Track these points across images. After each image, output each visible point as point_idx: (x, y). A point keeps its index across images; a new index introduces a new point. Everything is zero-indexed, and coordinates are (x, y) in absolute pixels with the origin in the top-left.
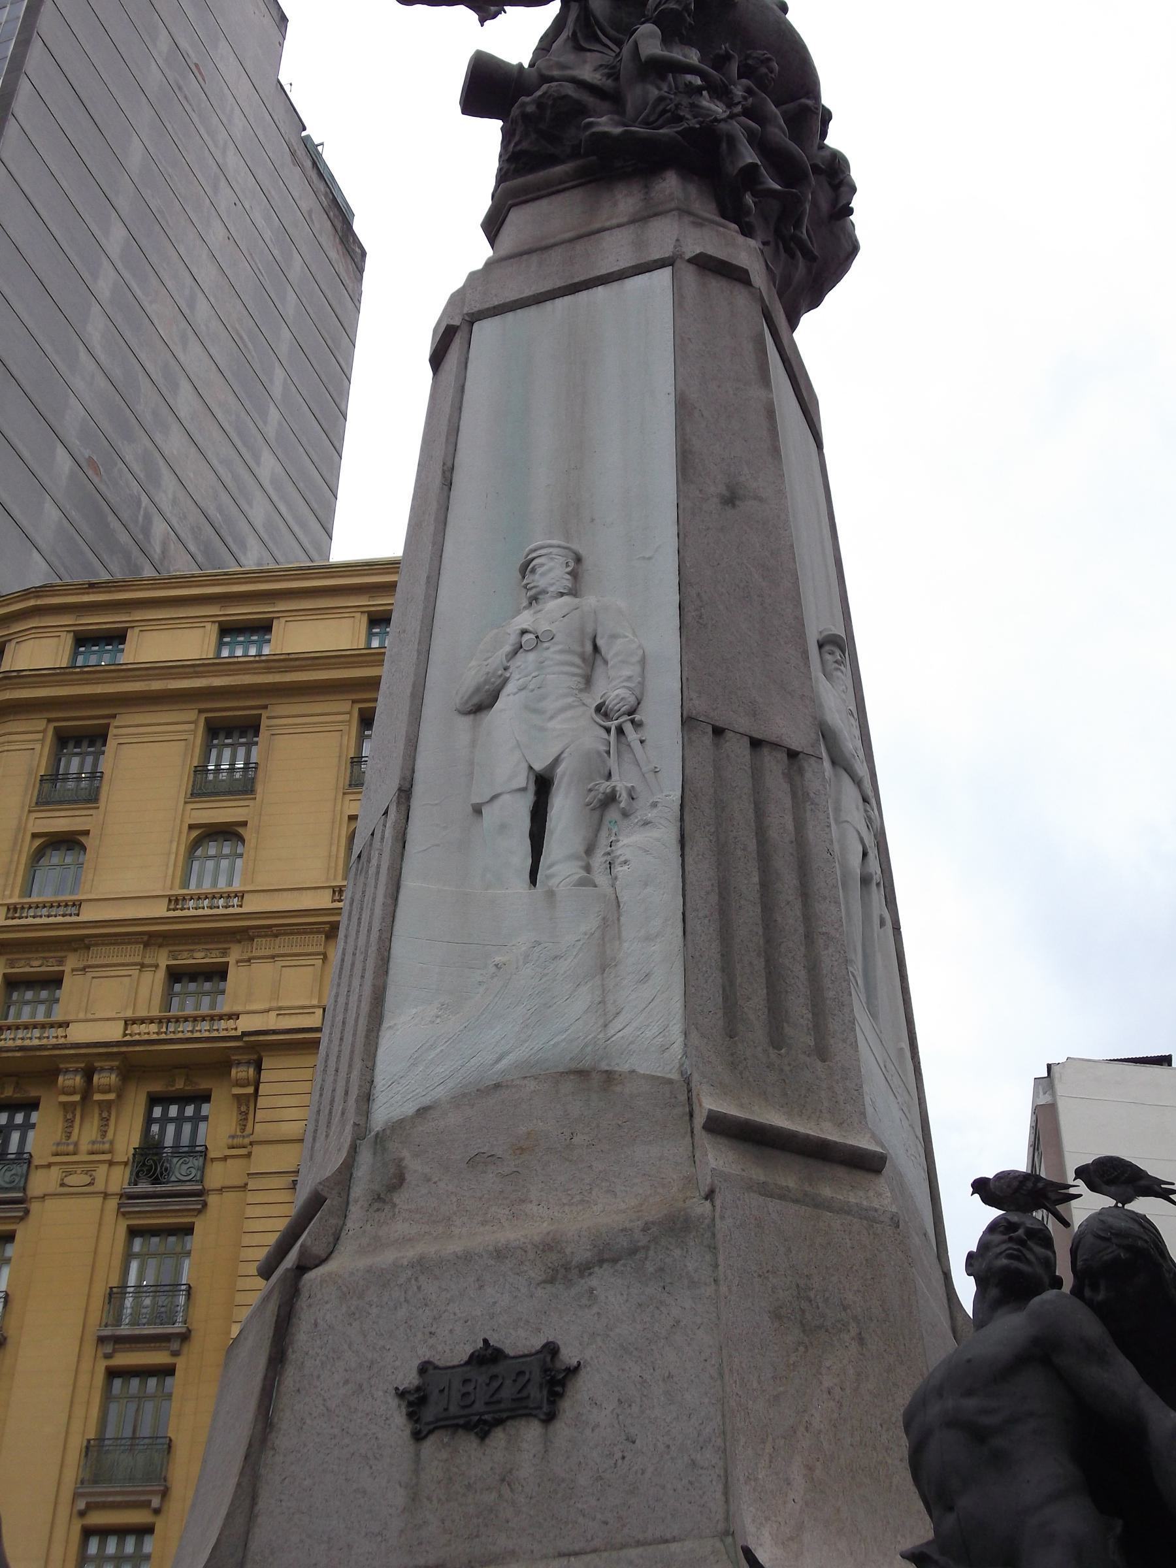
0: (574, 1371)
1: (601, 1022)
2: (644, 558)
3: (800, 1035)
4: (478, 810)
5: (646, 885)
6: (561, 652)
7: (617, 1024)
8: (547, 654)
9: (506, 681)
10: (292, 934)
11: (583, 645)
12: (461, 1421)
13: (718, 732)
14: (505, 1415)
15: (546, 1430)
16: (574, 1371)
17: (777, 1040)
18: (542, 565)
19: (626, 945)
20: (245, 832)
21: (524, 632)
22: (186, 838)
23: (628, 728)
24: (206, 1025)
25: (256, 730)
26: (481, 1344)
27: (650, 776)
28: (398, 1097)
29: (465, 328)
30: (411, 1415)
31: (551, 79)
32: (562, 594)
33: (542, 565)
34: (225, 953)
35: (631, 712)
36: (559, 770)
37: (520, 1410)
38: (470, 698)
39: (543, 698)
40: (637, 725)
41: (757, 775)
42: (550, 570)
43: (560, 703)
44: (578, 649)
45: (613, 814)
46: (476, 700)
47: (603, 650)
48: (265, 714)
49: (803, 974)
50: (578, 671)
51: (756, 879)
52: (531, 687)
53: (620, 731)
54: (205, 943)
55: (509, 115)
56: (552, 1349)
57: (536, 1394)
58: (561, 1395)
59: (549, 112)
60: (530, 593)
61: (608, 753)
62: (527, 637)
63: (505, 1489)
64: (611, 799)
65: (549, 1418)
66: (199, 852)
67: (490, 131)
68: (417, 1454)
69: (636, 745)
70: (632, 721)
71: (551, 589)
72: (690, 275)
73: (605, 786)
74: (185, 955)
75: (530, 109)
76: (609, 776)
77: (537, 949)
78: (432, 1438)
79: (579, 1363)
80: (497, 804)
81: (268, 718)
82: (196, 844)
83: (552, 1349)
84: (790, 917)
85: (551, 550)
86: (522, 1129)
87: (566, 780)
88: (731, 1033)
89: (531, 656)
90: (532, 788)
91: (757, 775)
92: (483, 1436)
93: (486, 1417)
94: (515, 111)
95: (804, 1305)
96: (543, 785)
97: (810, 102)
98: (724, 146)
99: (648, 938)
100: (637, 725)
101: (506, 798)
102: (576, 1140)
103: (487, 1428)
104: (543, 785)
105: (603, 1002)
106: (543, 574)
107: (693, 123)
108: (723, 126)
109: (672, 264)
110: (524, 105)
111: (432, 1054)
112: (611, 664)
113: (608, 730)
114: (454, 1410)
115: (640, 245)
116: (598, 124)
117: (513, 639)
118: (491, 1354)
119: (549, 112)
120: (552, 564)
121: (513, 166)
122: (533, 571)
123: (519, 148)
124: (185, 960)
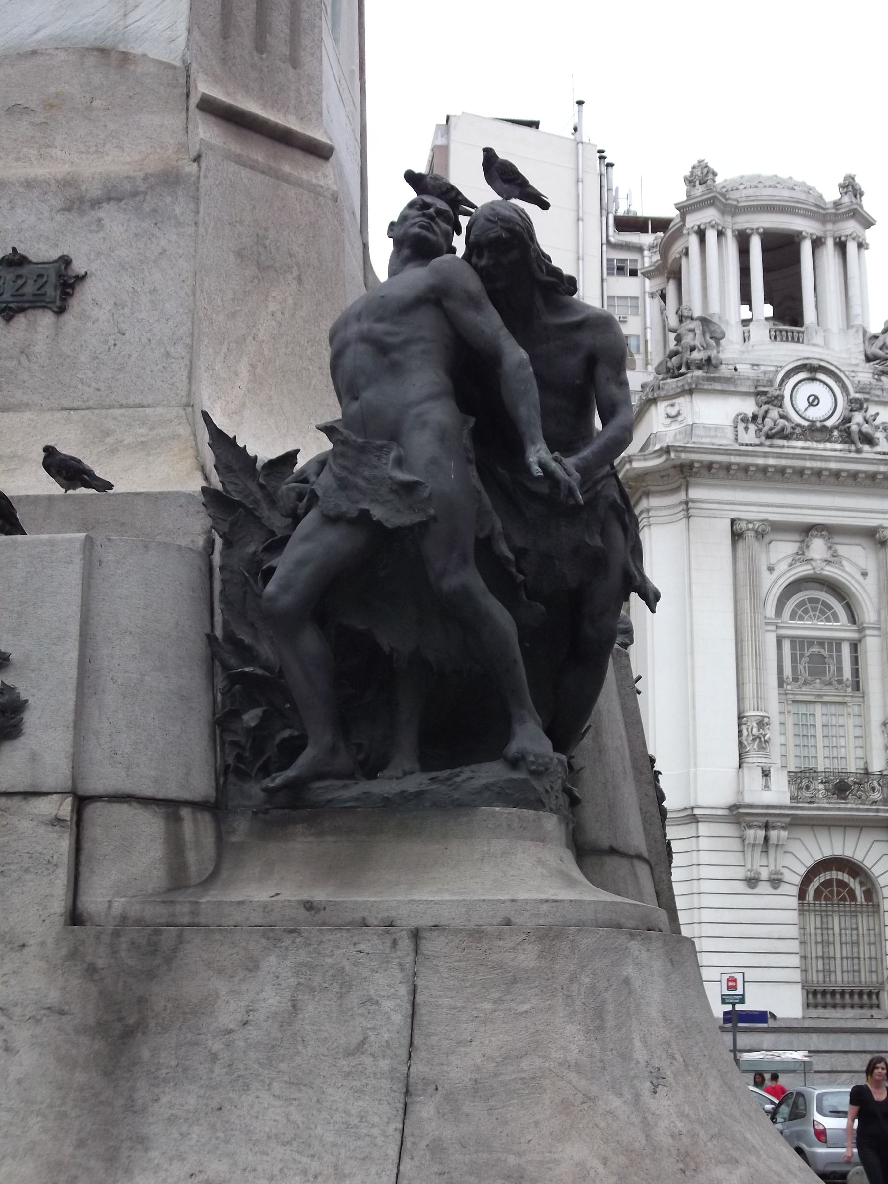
0: (81, 278)
1: (122, 12)
7: (134, 16)
14: (26, 305)
16: (81, 278)
26: (10, 251)
37: (38, 303)
56: (65, 261)
58: (70, 295)
63: (23, 359)
65: (61, 311)
79: (86, 273)
83: (65, 261)
86: (52, 90)
88: (225, 35)
93: (11, 305)
95: (261, 249)
102: (97, 103)
103: (11, 314)
118: (18, 259)
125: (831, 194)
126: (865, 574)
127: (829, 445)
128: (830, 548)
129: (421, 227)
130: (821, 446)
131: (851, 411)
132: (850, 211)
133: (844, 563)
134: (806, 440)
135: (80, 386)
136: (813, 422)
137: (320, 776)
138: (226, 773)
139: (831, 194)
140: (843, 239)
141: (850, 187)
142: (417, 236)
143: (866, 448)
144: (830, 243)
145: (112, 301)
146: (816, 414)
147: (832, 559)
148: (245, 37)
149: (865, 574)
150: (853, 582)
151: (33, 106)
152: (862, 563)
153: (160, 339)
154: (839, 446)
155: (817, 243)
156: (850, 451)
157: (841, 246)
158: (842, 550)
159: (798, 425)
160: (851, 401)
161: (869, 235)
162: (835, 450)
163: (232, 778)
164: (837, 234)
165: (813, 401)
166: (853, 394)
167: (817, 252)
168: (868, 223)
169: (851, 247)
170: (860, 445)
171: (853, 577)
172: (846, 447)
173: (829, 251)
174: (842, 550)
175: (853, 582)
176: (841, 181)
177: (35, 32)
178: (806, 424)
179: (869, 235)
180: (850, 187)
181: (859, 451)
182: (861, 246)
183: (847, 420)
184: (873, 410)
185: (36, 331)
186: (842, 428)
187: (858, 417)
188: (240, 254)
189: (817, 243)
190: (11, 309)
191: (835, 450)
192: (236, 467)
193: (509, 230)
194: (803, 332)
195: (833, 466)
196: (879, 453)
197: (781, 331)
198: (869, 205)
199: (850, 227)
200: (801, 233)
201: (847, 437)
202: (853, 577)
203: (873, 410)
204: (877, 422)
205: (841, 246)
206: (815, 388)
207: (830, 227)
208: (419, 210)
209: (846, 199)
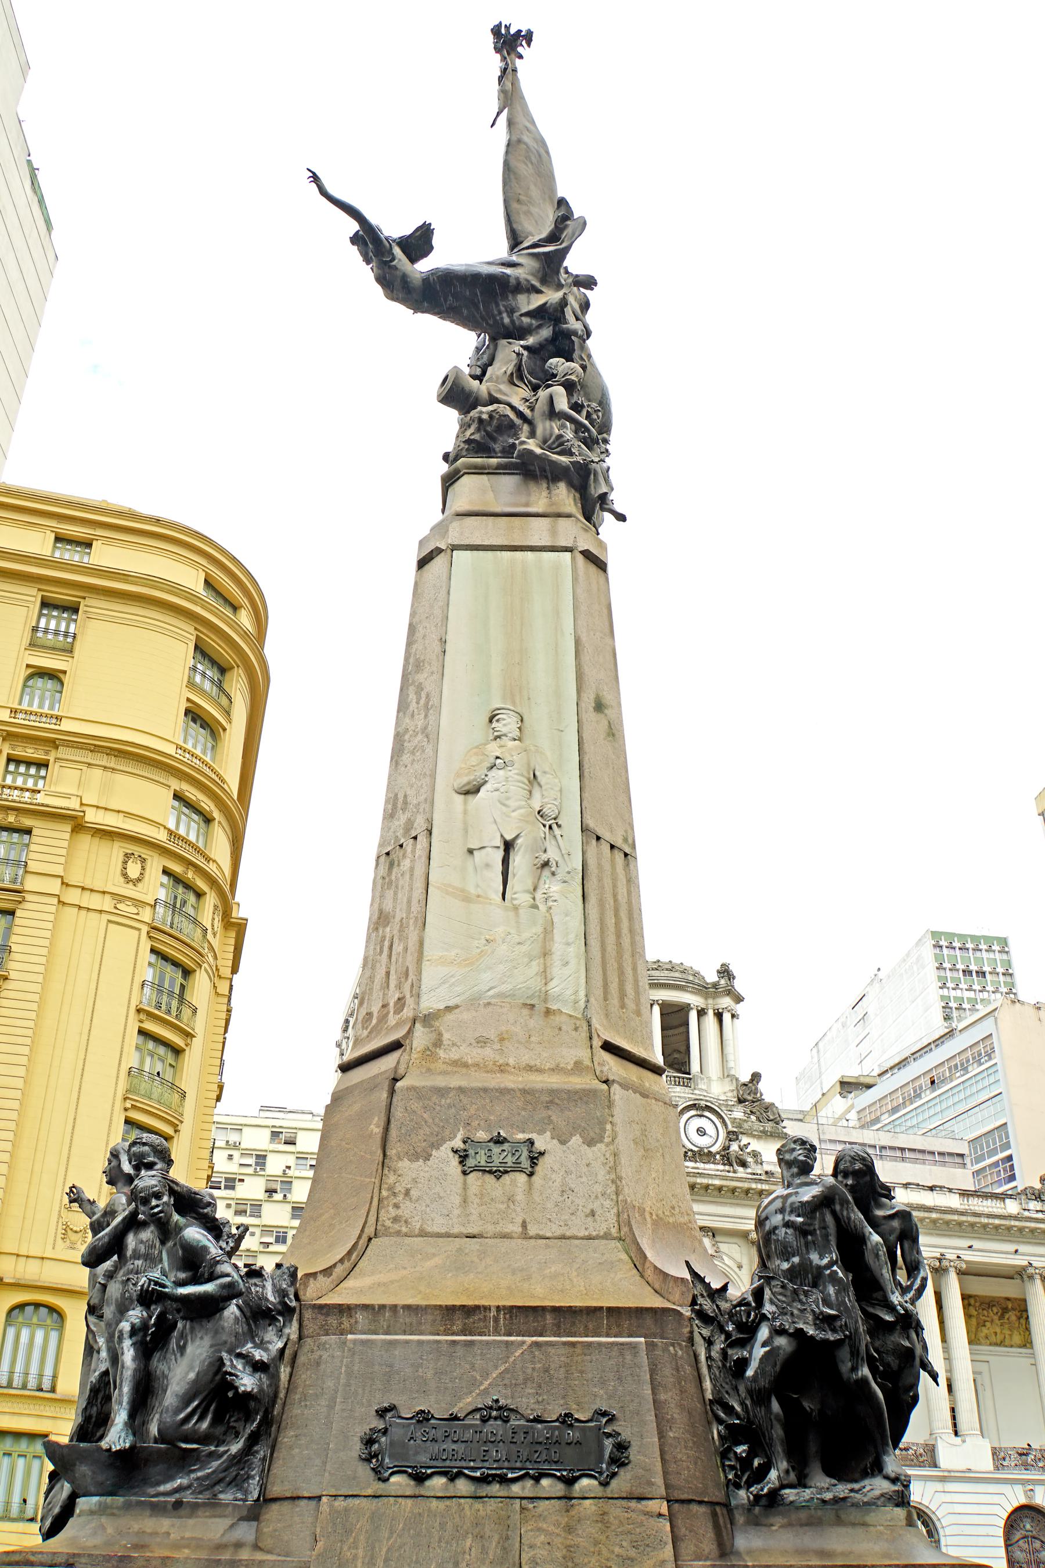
0: (542, 1154)
1: (544, 981)
2: (559, 730)
3: (631, 1005)
4: (471, 852)
5: (567, 915)
6: (518, 774)
7: (552, 984)
8: (510, 773)
9: (486, 782)
10: (82, 748)
11: (529, 773)
12: (487, 1169)
13: (612, 847)
14: (509, 1169)
15: (1033, 1355)
17: (623, 1006)
18: (504, 719)
19: (556, 945)
20: (66, 680)
21: (497, 758)
22: (23, 673)
23: (554, 826)
24: (27, 794)
25: (76, 610)
27: (566, 856)
28: (434, 998)
29: (449, 551)
30: (461, 1162)
31: (497, 401)
32: (515, 740)
33: (504, 719)
34: (47, 753)
35: (555, 819)
36: (519, 841)
38: (464, 786)
39: (508, 798)
40: (559, 826)
41: (613, 861)
42: (509, 724)
43: (517, 804)
44: (525, 774)
45: (546, 872)
46: (467, 788)
47: (539, 779)
48: (83, 603)
49: (631, 972)
50: (526, 787)
51: (613, 921)
52: (502, 791)
53: (550, 827)
54: (35, 744)
55: (468, 412)
57: (526, 1163)
58: (536, 1164)
59: (495, 421)
60: (496, 734)
61: (545, 838)
62: (499, 761)
63: (511, 1204)
64: (546, 864)
66: (30, 683)
67: (451, 417)
68: (465, 1183)
69: (559, 837)
70: (557, 823)
71: (510, 735)
72: (580, 559)
73: (544, 857)
74: (20, 749)
75: (485, 416)
76: (545, 851)
77: (510, 936)
78: (472, 1175)
80: (483, 851)
81: (86, 606)
82: (30, 677)
84: (626, 941)
85: (509, 712)
86: (504, 1028)
87: (522, 850)
88: (606, 999)
89: (501, 772)
90: (502, 848)
91: (613, 861)
92: (498, 1178)
94: (474, 413)
95: (644, 1138)
96: (508, 846)
97: (469, 280)
98: (592, 476)
99: (568, 944)
100: (559, 826)
101: (487, 849)
102: (533, 1039)
104: (508, 846)
105: (545, 971)
106: (505, 725)
107: (579, 459)
108: (594, 465)
109: (571, 551)
110: (481, 412)
111: (454, 980)
112: (544, 788)
113: (544, 826)
114: (483, 1163)
115: (554, 532)
116: (529, 444)
117: (492, 760)
119: (495, 421)
120: (509, 720)
121: (467, 447)
122: (498, 721)
123: (472, 437)
124: (19, 752)
125: (711, 977)
126: (740, 1267)
127: (712, 1166)
128: (714, 1245)
129: (805, 1156)
130: (707, 1166)
131: (730, 1140)
132: (726, 990)
133: (724, 1257)
134: (696, 1162)
135: (549, 1223)
136: (701, 1149)
137: (783, 1487)
138: (727, 1486)
139: (711, 977)
140: (720, 1011)
141: (725, 972)
142: (802, 1161)
143: (741, 1169)
144: (711, 1012)
145: (563, 1169)
146: (703, 1142)
147: (715, 1254)
148: (615, 1001)
149: (740, 1267)
150: (731, 1272)
151: (492, 1038)
152: (737, 1256)
153: (564, 1184)
154: (721, 1167)
155: (701, 1013)
156: (729, 1172)
157: (719, 1016)
158: (723, 1247)
159: (691, 1150)
160: (729, 1133)
161: (739, 1008)
162: (718, 1170)
163: (731, 1487)
164: (716, 1007)
165: (701, 1132)
166: (730, 1128)
167: (702, 1019)
168: (739, 999)
169: (726, 1017)
170: (736, 1167)
171: (731, 1269)
172: (727, 1168)
173: (710, 1019)
174: (723, 1247)
175: (731, 1272)
176: (719, 967)
177: (489, 990)
178: (696, 1149)
179: (739, 1008)
180: (725, 972)
181: (735, 1172)
182: (733, 1016)
183: (726, 1148)
184: (745, 1140)
185: (517, 1186)
186: (723, 1153)
187: (734, 1147)
188: (636, 1143)
189: (701, 1013)
190: (500, 1171)
191: (718, 1170)
192: (705, 1294)
193: (865, 1165)
194: (690, 1079)
195: (717, 1182)
196: (751, 1174)
197: (675, 1077)
198: (739, 985)
199: (726, 1002)
200: (689, 1004)
201: (727, 1158)
202: (731, 1269)
203: (745, 1140)
204: (748, 1150)
205: (719, 1016)
206: (702, 1122)
207: (710, 1001)
208: (800, 1145)
209: (723, 982)
